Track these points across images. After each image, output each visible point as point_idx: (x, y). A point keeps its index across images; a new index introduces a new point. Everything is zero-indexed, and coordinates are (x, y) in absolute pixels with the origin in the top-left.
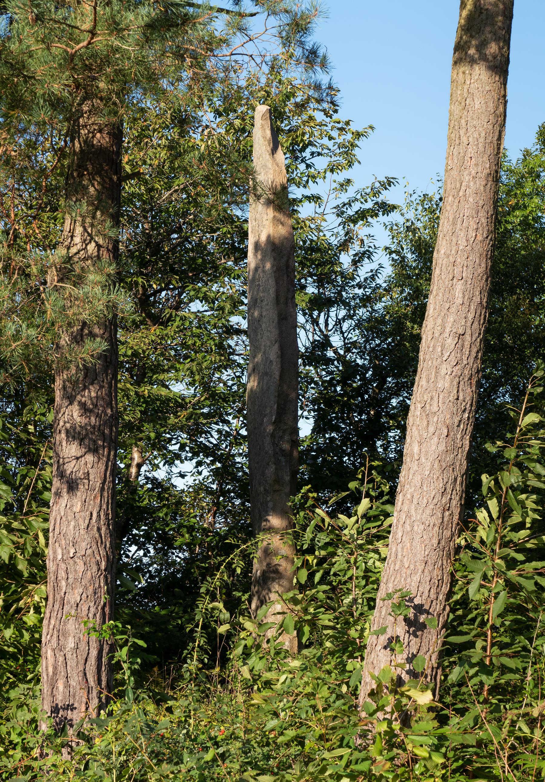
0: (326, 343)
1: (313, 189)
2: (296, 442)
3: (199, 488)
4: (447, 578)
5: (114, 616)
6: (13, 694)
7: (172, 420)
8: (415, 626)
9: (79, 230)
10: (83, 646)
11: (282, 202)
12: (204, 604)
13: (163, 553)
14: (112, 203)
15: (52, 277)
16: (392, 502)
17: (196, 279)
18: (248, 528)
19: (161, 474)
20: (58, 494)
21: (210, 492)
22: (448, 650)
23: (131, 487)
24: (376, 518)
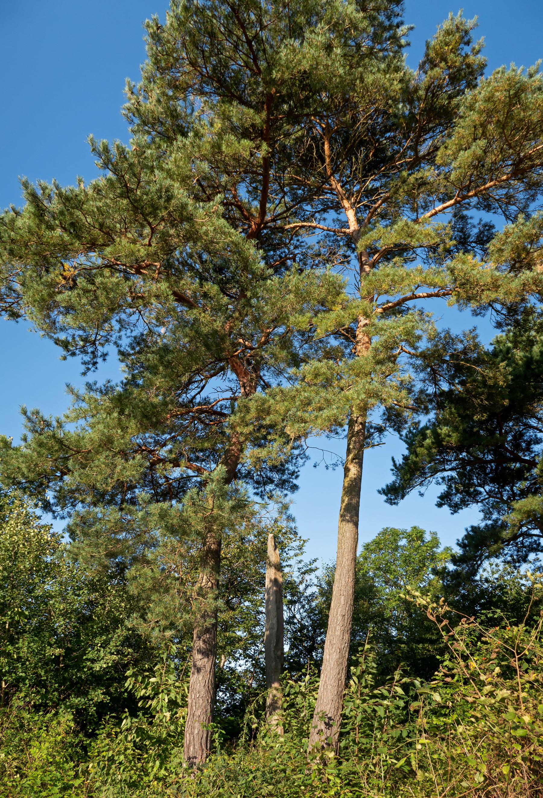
0: (294, 617)
1: (289, 563)
2: (283, 653)
3: (246, 671)
4: (341, 707)
5: (213, 721)
6: (172, 752)
7: (237, 645)
8: (328, 725)
9: (205, 577)
10: (201, 732)
11: (279, 568)
12: (247, 716)
13: (232, 696)
14: (217, 569)
15: (194, 595)
16: (319, 676)
17: (247, 594)
18: (265, 686)
19: (232, 665)
20: (193, 673)
21: (251, 672)
22: (341, 735)
23: (221, 670)
24: (313, 683)
